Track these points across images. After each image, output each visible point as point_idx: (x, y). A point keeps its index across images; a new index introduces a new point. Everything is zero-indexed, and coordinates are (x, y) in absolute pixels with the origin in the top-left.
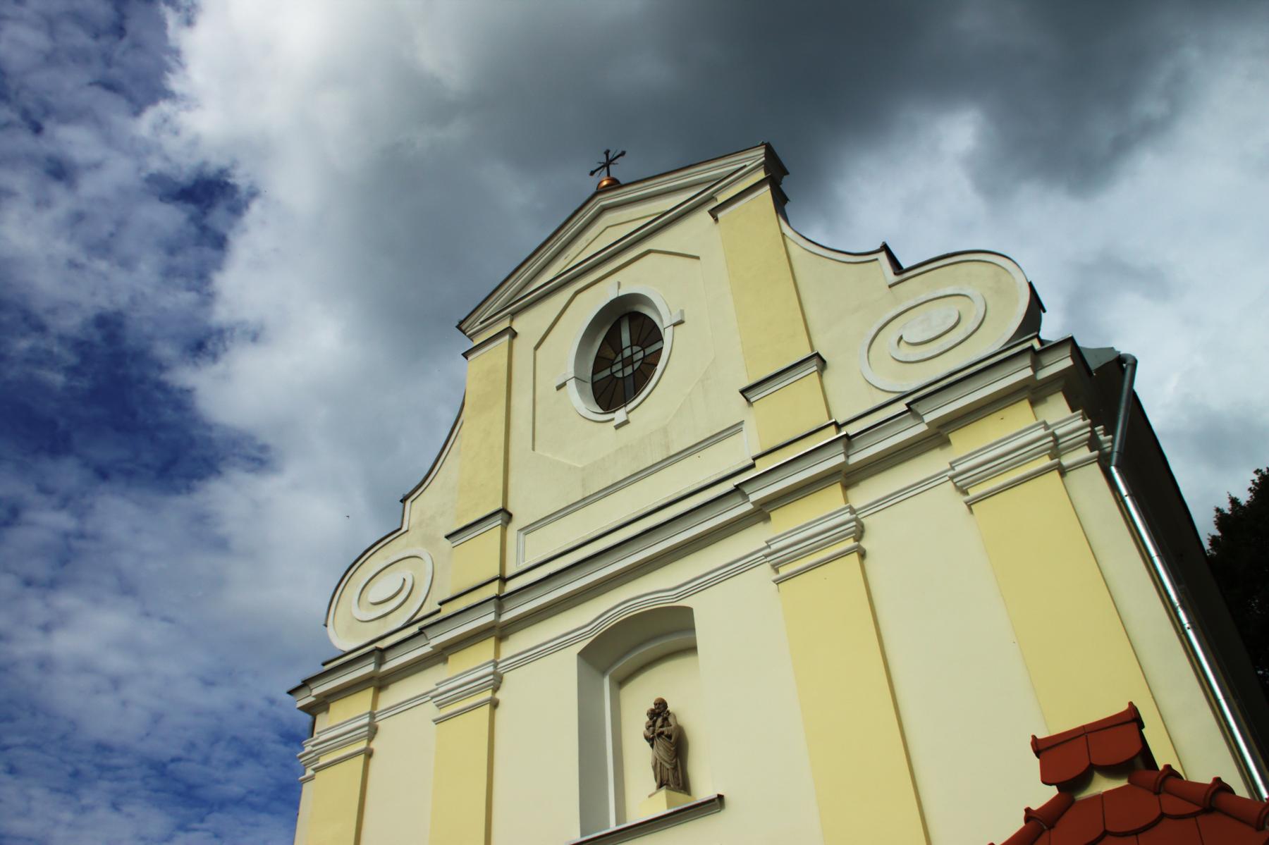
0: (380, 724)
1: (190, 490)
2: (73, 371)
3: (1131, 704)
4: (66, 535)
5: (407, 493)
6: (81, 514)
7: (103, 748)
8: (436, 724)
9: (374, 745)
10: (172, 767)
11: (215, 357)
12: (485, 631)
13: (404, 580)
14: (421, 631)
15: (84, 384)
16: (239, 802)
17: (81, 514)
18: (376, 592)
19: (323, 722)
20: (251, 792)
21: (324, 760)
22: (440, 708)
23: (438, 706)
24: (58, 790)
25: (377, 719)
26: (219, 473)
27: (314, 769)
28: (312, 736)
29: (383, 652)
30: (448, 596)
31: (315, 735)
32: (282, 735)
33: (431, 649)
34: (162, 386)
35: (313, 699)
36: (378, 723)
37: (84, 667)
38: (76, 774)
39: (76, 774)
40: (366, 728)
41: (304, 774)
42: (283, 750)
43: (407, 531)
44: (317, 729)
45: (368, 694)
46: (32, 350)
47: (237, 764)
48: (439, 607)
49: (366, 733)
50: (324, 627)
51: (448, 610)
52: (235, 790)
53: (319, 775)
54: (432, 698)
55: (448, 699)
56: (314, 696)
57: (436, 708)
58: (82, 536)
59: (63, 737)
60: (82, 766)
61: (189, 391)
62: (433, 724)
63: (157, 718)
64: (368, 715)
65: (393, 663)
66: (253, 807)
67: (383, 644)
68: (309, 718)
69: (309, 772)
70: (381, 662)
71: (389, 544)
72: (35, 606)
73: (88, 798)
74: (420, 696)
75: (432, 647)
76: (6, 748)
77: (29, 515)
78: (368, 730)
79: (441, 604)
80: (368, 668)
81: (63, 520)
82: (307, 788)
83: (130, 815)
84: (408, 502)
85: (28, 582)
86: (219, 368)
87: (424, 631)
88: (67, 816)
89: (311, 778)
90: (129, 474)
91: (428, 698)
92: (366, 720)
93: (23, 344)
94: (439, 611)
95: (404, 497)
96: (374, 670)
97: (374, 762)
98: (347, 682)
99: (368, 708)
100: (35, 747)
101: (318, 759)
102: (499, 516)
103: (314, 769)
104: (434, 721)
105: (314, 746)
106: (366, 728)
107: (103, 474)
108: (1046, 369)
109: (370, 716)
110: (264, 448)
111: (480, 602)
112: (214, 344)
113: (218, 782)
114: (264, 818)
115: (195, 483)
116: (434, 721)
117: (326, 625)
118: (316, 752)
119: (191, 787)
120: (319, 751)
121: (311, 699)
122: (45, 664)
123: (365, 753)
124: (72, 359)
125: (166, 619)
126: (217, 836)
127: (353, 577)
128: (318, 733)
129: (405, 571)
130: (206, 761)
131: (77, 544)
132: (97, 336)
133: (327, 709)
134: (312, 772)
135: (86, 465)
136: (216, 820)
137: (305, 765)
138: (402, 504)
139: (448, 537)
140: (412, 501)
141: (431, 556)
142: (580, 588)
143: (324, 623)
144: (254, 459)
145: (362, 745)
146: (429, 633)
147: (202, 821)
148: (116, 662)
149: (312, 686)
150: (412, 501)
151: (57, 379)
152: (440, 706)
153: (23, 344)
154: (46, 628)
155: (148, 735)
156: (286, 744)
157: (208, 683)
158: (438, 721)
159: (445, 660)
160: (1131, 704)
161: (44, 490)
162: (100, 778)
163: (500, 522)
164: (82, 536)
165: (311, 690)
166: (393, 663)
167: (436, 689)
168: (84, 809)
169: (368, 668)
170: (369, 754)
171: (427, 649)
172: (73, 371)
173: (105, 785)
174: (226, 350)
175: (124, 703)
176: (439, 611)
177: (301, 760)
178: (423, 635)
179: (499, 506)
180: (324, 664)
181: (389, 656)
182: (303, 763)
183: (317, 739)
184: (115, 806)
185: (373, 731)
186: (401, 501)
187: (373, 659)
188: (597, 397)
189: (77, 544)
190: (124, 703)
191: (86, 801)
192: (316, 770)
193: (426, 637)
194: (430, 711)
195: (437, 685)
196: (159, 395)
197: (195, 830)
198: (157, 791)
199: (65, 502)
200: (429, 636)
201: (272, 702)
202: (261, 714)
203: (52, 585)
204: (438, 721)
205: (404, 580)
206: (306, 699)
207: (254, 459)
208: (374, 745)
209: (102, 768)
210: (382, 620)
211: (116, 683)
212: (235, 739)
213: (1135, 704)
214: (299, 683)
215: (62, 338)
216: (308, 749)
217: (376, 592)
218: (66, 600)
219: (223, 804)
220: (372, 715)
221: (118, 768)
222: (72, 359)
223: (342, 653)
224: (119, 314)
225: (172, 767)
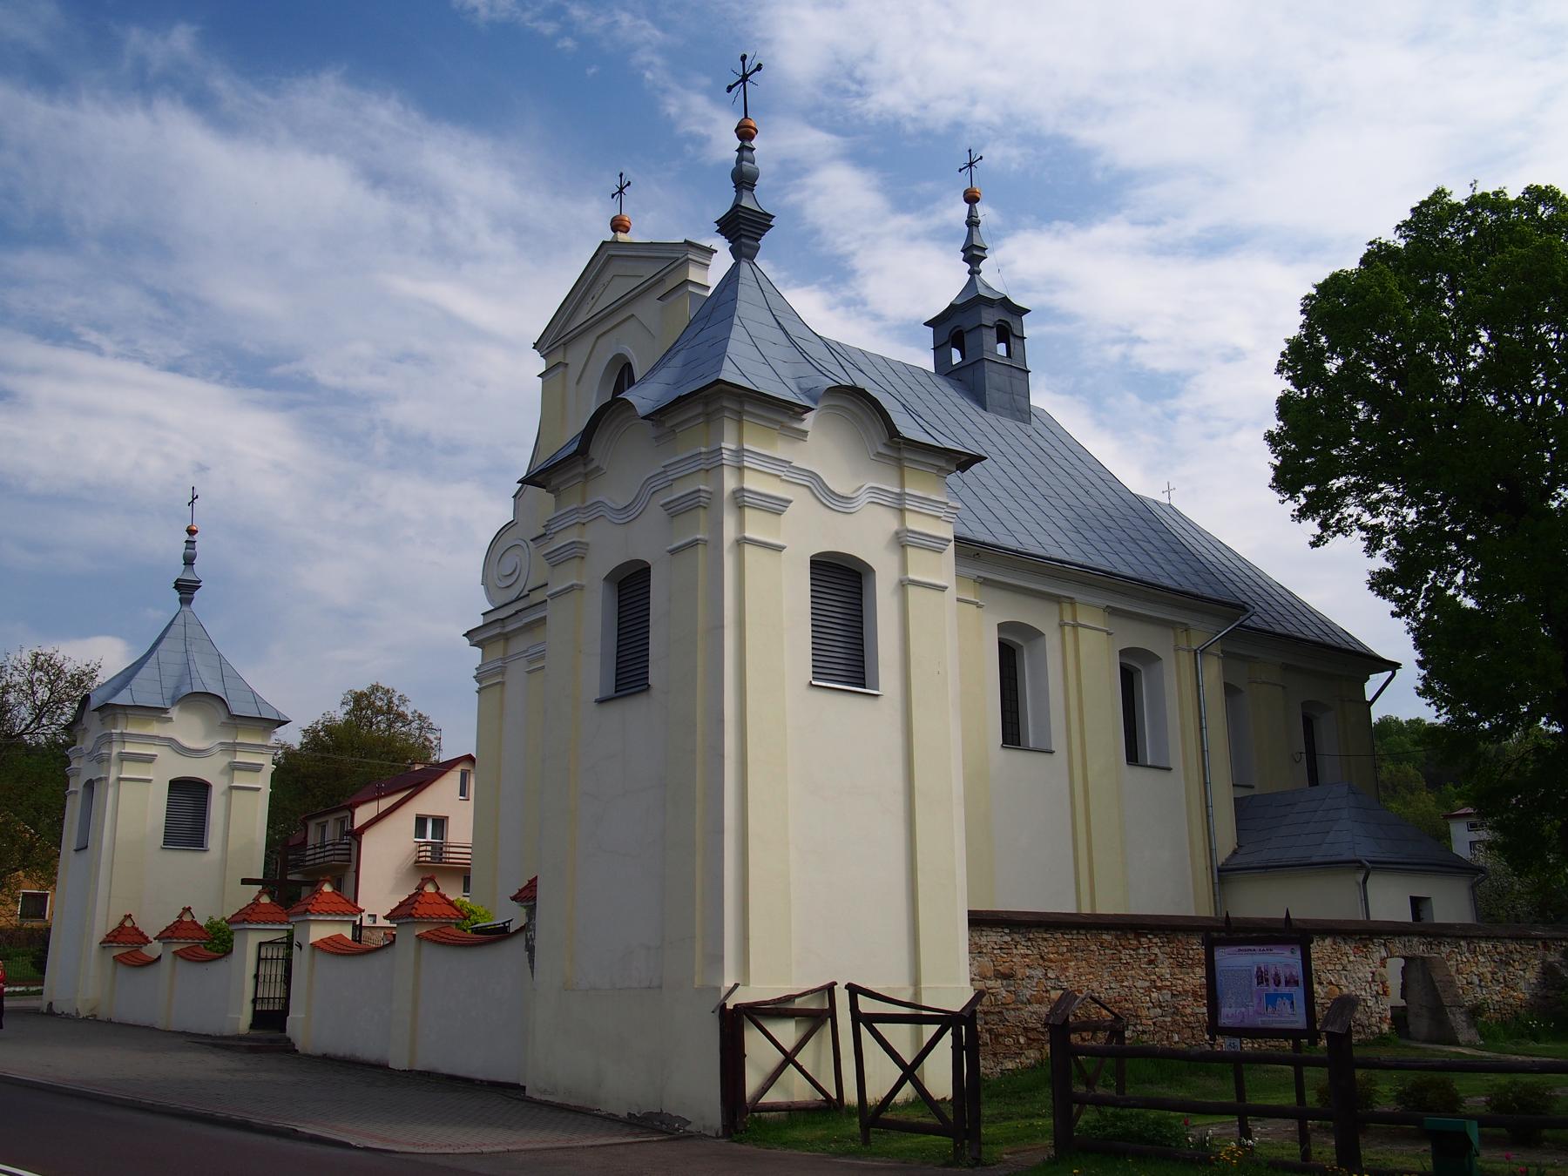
158: (528, 672)
171: (519, 624)
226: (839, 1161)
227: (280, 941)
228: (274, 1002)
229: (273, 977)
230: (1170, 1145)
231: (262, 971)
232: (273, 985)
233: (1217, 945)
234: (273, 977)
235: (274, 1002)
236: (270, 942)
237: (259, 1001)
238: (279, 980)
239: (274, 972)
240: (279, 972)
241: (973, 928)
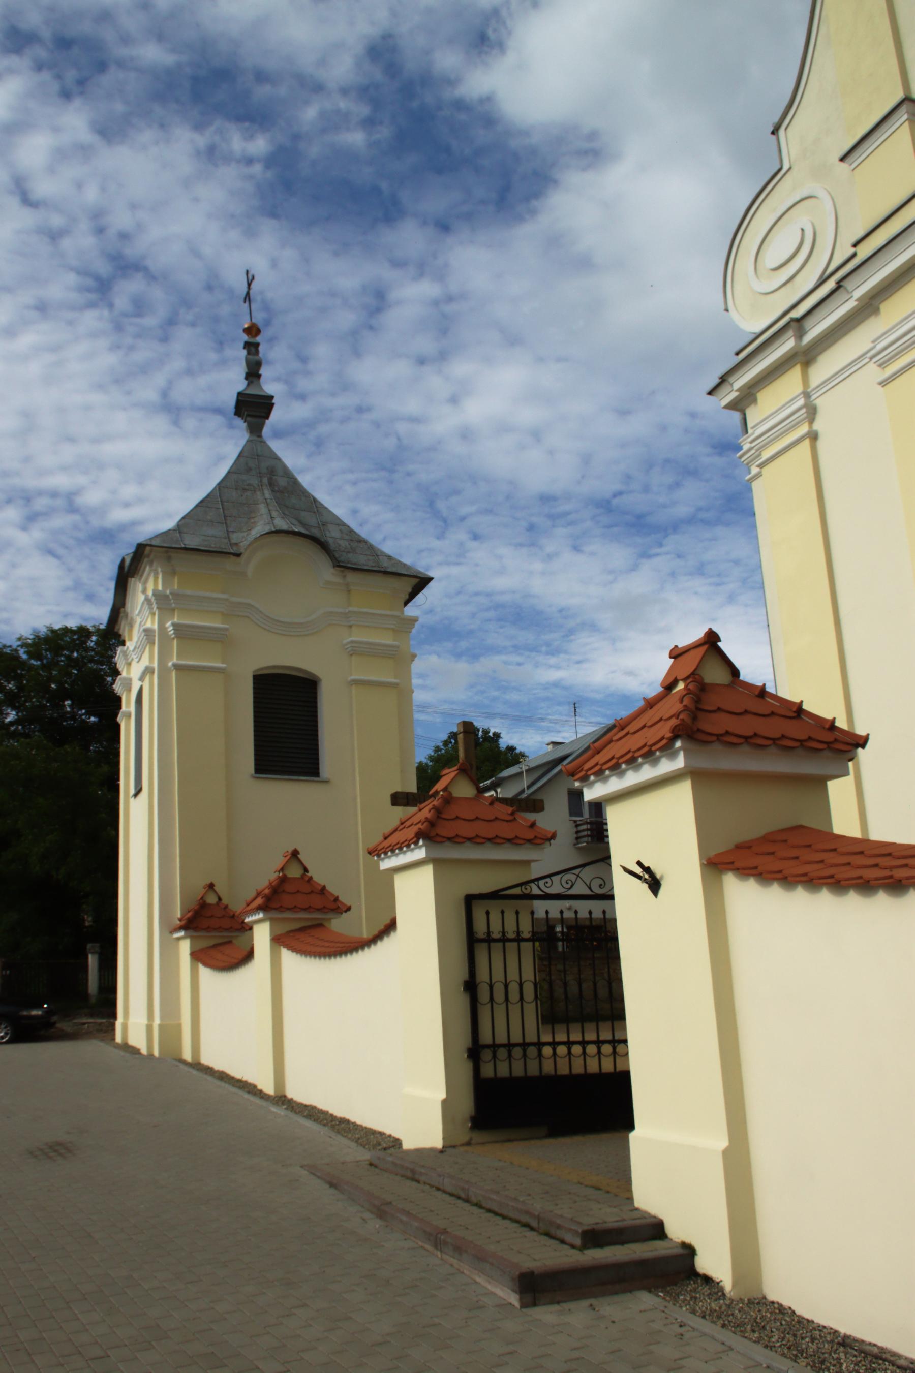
0: (818, 402)
1: (533, 213)
2: (369, 123)
3: (868, 735)
4: (436, 303)
5: (776, 119)
6: (441, 276)
7: (546, 499)
8: (883, 386)
9: (817, 426)
10: (615, 502)
11: (501, 46)
12: (900, 276)
13: (802, 230)
14: (839, 286)
15: (385, 132)
16: (691, 521)
17: (441, 276)
18: (775, 253)
19: (754, 415)
20: (700, 509)
21: (766, 455)
22: (884, 368)
23: (880, 366)
24: (521, 545)
25: (813, 397)
26: (555, 182)
27: (758, 466)
28: (747, 432)
29: (799, 320)
30: (861, 233)
31: (750, 431)
32: (714, 447)
33: (856, 303)
34: (460, 105)
35: (737, 394)
36: (815, 402)
37: (503, 428)
38: (531, 528)
39: (531, 528)
40: (804, 410)
41: (750, 473)
42: (719, 461)
43: (790, 169)
44: (750, 425)
45: (796, 373)
46: (322, 114)
47: (677, 485)
48: (853, 250)
49: (805, 415)
50: (726, 313)
51: (864, 251)
52: (682, 511)
53: (765, 470)
54: (871, 358)
55: (889, 356)
56: (737, 391)
57: (878, 368)
58: (450, 299)
59: (508, 497)
60: (534, 520)
61: (488, 99)
62: (880, 387)
63: (586, 459)
64: (802, 396)
65: (815, 329)
66: (707, 523)
67: (797, 313)
68: (736, 416)
69: (754, 470)
70: (800, 334)
71: (772, 193)
72: (435, 383)
73: (550, 547)
74: (856, 360)
75: (857, 300)
76: (463, 519)
77: (394, 295)
78: (806, 412)
79: (855, 245)
80: (787, 345)
81: (427, 289)
82: (755, 485)
83: (592, 554)
84: (782, 132)
85: (422, 361)
86: (511, 58)
87: (842, 283)
88: (538, 566)
89: (758, 475)
90: (468, 217)
91: (867, 360)
92: (801, 402)
93: (310, 114)
94: (854, 255)
95: (775, 127)
96: (795, 345)
97: (821, 444)
98: (758, 375)
99: (800, 389)
100: (489, 511)
101: (760, 455)
102: (904, 108)
103: (758, 466)
104: (880, 384)
105: (751, 442)
106: (804, 410)
107: (444, 227)
108: (809, 332)
109: (804, 397)
110: (593, 136)
111: (904, 228)
112: (495, 30)
113: (664, 506)
114: (719, 531)
115: (535, 203)
116: (880, 384)
117: (727, 310)
118: (755, 448)
119: (640, 517)
120: (759, 446)
121: (734, 395)
122: (466, 434)
123: (810, 437)
124: (364, 110)
125: (559, 360)
126: (679, 556)
127: (741, 245)
128: (752, 428)
129: (801, 219)
130: (646, 489)
131: (448, 309)
132: (378, 75)
133: (755, 401)
134: (758, 469)
135: (425, 223)
136: (673, 542)
137: (748, 464)
138: (774, 137)
139: (842, 159)
140: (786, 129)
141: (828, 191)
142: (823, 331)
143: (723, 307)
144: (585, 153)
145: (804, 429)
146: (847, 284)
147: (661, 545)
148: (529, 416)
149: (731, 380)
150: (786, 129)
151: (356, 138)
152: (882, 365)
153: (310, 114)
154: (454, 400)
155: (583, 477)
156: (720, 454)
157: (623, 413)
158: (884, 383)
159: (876, 311)
160: (868, 735)
161: (398, 264)
162: (554, 526)
163: (905, 117)
164: (450, 299)
165: (732, 385)
166: (815, 329)
167: (874, 347)
168: (550, 557)
169: (787, 345)
170: (813, 437)
171: (851, 304)
172: (369, 123)
173: (560, 531)
174: (510, 33)
175: (551, 452)
176: (854, 255)
177: (743, 459)
178: (841, 289)
179: (900, 95)
180: (737, 354)
181: (808, 323)
182: (745, 462)
183: (753, 434)
184: (576, 549)
185: (812, 412)
186: (773, 133)
187: (790, 333)
188: (105, 769)
189: (448, 309)
190: (551, 452)
191: (550, 548)
192: (761, 466)
193: (729, 383)
194: (873, 373)
195: (873, 342)
196: (462, 117)
197: (657, 555)
198: (609, 527)
199: (422, 269)
200: (850, 288)
201: (693, 415)
202: (687, 431)
203: (443, 356)
204: (884, 383)
205: (802, 230)
206: (729, 395)
207: (585, 153)
208: (817, 426)
209: (552, 517)
210: (789, 285)
211: (536, 435)
212: (667, 461)
213: (870, 737)
214: (716, 381)
215: (344, 91)
216: (746, 447)
217: (775, 253)
218: (461, 368)
219: (675, 527)
220: (807, 395)
221: (567, 514)
222: (364, 110)
223: (753, 336)
224: (387, 36)
225: (615, 502)
226: (848, 739)
227: (517, 891)
228: (540, 1055)
229: (514, 988)
230: (355, 483)
231: (482, 975)
232: (515, 1011)
233: (114, 627)
234: (514, 988)
235: (525, 1056)
236: (494, 895)
237: (487, 1055)
238: (529, 990)
239: (513, 975)
240: (529, 973)
241: (462, 725)
